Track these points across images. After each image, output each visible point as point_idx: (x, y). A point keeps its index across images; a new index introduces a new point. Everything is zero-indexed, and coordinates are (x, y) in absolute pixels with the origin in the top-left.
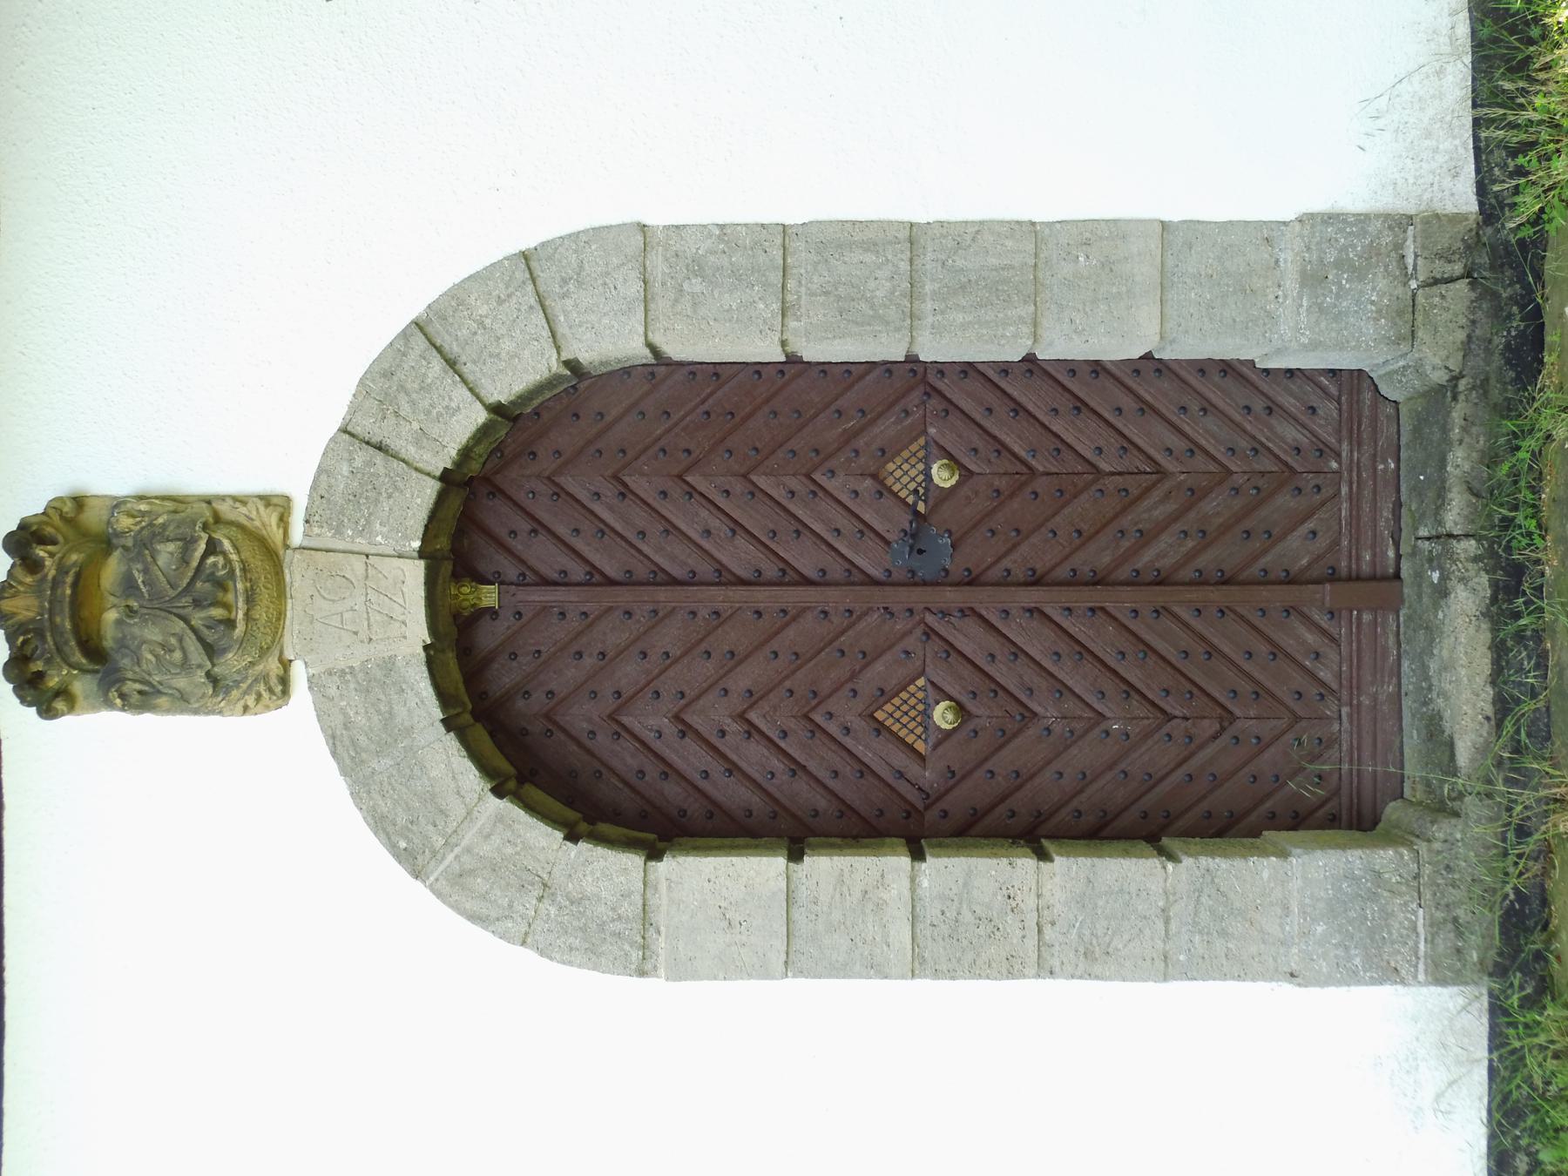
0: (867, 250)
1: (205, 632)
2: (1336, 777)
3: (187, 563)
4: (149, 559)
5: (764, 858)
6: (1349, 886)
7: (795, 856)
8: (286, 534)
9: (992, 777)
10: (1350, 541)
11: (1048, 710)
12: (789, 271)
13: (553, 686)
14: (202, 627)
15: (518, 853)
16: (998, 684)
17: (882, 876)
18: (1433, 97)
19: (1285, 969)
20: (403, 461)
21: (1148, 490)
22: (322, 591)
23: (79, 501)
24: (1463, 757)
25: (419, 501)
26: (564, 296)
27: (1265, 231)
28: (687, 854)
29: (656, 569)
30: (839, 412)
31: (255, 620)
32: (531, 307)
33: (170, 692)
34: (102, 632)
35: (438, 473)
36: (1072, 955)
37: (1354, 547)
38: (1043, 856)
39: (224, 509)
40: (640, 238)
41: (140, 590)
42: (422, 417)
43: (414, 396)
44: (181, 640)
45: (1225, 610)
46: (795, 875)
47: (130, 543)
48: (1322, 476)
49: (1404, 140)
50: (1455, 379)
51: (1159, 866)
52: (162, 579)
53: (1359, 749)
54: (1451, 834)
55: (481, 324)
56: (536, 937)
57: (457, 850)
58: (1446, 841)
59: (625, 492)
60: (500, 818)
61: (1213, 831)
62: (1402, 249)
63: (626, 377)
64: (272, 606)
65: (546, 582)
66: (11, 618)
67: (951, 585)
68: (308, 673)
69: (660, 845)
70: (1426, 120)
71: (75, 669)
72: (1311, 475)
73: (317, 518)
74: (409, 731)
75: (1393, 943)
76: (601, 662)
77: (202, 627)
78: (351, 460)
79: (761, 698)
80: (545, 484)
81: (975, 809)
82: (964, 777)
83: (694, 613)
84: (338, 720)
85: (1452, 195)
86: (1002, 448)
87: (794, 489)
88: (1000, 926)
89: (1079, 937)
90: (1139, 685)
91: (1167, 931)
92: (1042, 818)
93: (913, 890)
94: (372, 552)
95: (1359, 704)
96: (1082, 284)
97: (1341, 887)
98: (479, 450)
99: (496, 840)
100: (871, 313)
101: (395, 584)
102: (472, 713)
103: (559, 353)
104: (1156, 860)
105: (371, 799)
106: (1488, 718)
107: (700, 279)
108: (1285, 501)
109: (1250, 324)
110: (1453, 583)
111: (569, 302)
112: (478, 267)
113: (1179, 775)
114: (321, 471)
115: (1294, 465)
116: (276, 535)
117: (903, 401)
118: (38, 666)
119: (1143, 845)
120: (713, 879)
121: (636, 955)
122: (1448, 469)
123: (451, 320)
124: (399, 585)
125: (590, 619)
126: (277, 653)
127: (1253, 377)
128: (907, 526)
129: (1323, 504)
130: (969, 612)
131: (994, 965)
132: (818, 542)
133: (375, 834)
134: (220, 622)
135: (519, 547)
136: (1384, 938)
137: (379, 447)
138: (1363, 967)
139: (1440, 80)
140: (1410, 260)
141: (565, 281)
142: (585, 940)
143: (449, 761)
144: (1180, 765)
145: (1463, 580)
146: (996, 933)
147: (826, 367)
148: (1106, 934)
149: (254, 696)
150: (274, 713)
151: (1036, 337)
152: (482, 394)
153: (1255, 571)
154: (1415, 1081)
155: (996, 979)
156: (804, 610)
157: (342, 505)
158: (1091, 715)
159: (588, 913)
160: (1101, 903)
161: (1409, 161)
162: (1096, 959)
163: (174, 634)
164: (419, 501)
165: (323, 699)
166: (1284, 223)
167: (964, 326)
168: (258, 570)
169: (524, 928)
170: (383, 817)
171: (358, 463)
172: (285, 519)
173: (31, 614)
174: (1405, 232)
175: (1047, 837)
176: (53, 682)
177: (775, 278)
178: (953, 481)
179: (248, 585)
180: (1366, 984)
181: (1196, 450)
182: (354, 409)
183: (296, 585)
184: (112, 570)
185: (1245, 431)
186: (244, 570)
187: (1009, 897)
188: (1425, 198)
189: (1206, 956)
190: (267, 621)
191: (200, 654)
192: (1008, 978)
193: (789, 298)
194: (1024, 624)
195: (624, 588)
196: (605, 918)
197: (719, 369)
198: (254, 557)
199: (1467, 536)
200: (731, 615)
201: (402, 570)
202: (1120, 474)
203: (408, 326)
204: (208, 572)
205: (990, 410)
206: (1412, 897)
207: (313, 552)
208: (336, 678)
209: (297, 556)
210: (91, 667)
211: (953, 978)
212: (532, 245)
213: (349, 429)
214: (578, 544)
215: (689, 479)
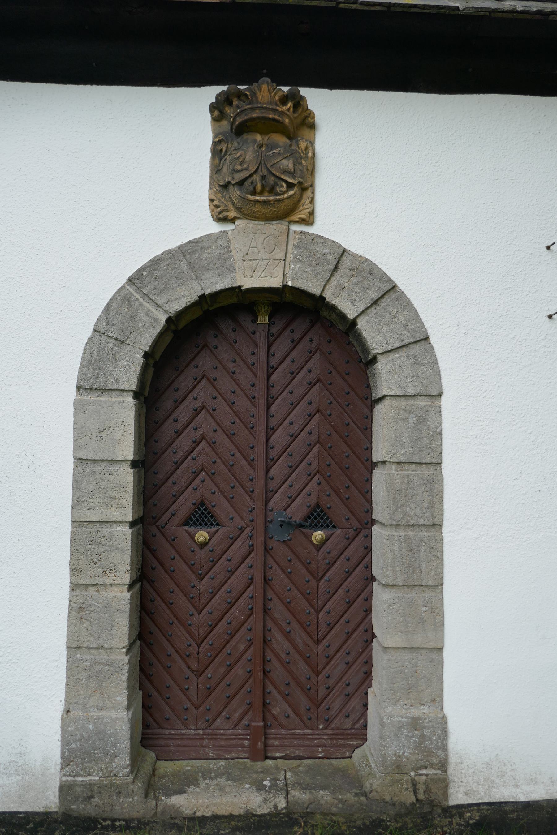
0: (429, 503)
1: (249, 181)
2: (169, 727)
3: (283, 173)
4: (285, 156)
5: (133, 449)
6: (112, 741)
7: (134, 464)
8: (296, 222)
9: (171, 559)
10: (284, 734)
11: (204, 586)
12: (419, 465)
13: (220, 348)
15: (139, 329)
16: (217, 562)
17: (123, 507)
18: (504, 782)
19: (71, 708)
20: (330, 279)
21: (309, 634)
23: (312, 127)
24: (177, 800)
25: (310, 285)
26: (408, 356)
27: (438, 699)
28: (136, 411)
29: (275, 398)
30: (348, 487)
31: (255, 205)
32: (403, 341)
33: (221, 164)
35: (324, 295)
36: (81, 601)
37: (281, 736)
38: (131, 586)
39: (309, 193)
40: (435, 393)
41: (271, 151)
42: (351, 288)
43: (361, 284)
44: (246, 169)
45: (251, 673)
46: (125, 464)
47: (293, 147)
48: (316, 721)
49: (483, 768)
50: (365, 794)
51: (125, 645)
52: (276, 161)
53: (182, 739)
54: (137, 794)
55: (395, 317)
56: (98, 337)
57: (141, 300)
58: (133, 791)
59: (311, 385)
60: (156, 320)
61: (143, 666)
62: (431, 767)
63: (366, 386)
65: (269, 346)
66: (258, 89)
67: (265, 540)
69: (142, 398)
70: (493, 778)
71: (233, 120)
72: (316, 715)
73: (303, 237)
74: (198, 278)
75: (82, 764)
76: (230, 371)
77: (252, 179)
78: (330, 254)
79: (212, 448)
80: (316, 346)
81: (156, 550)
82: (171, 545)
83: (253, 416)
84: (205, 244)
85: (457, 792)
86: (330, 565)
87: (312, 465)
88: (96, 566)
89: (90, 605)
90: (215, 631)
91: (92, 648)
92: (151, 583)
93: (115, 522)
95: (203, 739)
96: (412, 609)
97: (111, 737)
98: (334, 316)
99: (145, 318)
100: (399, 505)
102: (208, 310)
103: (380, 354)
104: (127, 643)
105: (167, 259)
106: (195, 813)
107: (415, 422)
108: (304, 702)
109: (392, 691)
110: (263, 794)
111: (405, 359)
112: (422, 316)
113: (171, 650)
114: (325, 239)
115: (321, 707)
116: (295, 217)
117: (353, 518)
118: (235, 102)
119: (136, 633)
120: (123, 423)
121: (87, 385)
122: (321, 792)
123: (397, 302)
125: (251, 367)
126: (239, 216)
127: (363, 687)
128: (294, 519)
129: (302, 721)
130: (251, 548)
131: (77, 562)
133: (150, 260)
134: (255, 188)
135: (286, 334)
136: (85, 759)
137: (336, 268)
138: (71, 748)
139: (513, 786)
140: (424, 772)
141: (415, 357)
142: (95, 361)
143: (184, 297)
144: (175, 649)
145: (265, 800)
146: (93, 563)
147: (370, 481)
148: (91, 618)
149: (218, 204)
150: (210, 215)
151: (386, 586)
152: (361, 317)
153: (270, 688)
154: (11, 774)
155: (70, 563)
156: (254, 469)
157: (309, 249)
158: (201, 608)
159: (109, 362)
160: (107, 616)
161: (473, 770)
162: (78, 613)
164: (310, 285)
165: (216, 237)
166: (442, 709)
167: (392, 551)
168: (279, 208)
169: (102, 331)
170: (158, 265)
171: (329, 257)
174: (439, 769)
175: (142, 585)
176: (228, 110)
177: (416, 459)
178: (315, 542)
179: (272, 202)
180: (62, 750)
181: (329, 659)
182: (354, 255)
183: (271, 226)
184: (281, 140)
185: (338, 683)
186: (279, 200)
187: (111, 570)
188: (455, 778)
189: (79, 668)
190: (254, 211)
191: (239, 178)
192: (70, 568)
193: (406, 465)
194: (245, 575)
195: (266, 383)
196: (106, 370)
197: (369, 430)
198: (285, 206)
199: (287, 802)
200: (252, 434)
201: (277, 277)
202: (318, 622)
203: (394, 282)
204: (279, 183)
205: (348, 560)
206: (105, 773)
207: (287, 234)
209: (285, 227)
210: (234, 127)
211: (71, 541)
212: (432, 342)
213: (345, 253)
214: (288, 361)
215: (317, 415)
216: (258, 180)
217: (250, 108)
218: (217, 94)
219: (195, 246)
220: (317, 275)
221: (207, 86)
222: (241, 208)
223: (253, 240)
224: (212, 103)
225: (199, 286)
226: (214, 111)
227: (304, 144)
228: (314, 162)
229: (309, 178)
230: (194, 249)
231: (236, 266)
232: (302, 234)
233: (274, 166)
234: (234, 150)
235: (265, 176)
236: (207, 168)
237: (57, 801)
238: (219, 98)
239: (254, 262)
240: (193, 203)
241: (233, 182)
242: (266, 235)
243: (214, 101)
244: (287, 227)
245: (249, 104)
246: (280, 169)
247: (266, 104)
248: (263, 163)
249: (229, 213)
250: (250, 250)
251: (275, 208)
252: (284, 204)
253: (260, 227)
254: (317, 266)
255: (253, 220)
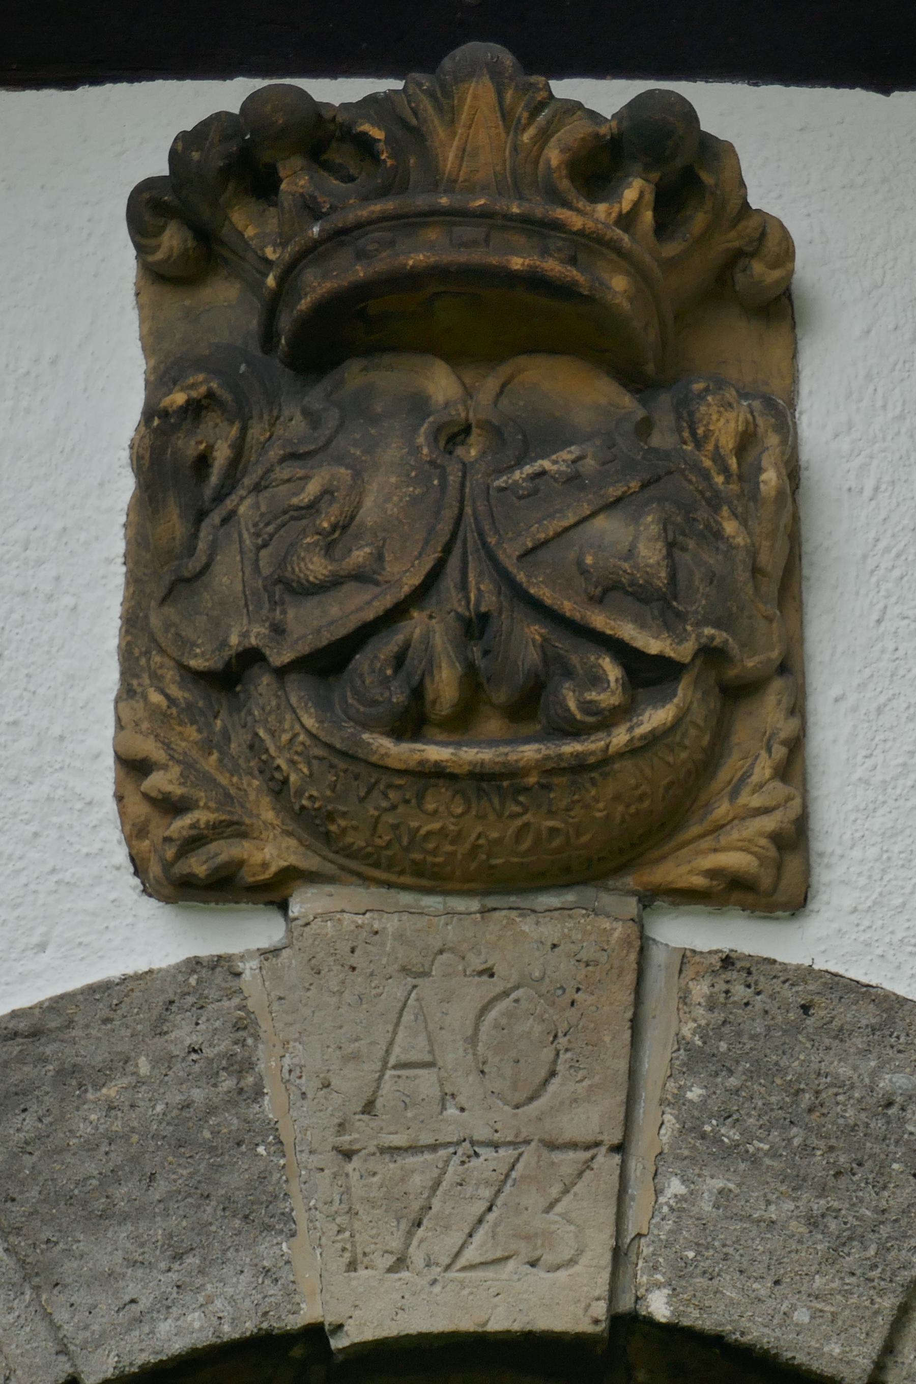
3: (598, 601)
4: (613, 492)
14: (400, 638)
22: (505, 1004)
25: (802, 1316)
31: (421, 797)
33: (202, 546)
34: (387, 359)
41: (520, 463)
44: (361, 577)
64: (462, 849)
66: (439, 108)
68: (242, 957)
71: (281, 281)
73: (740, 992)
77: (400, 638)
94: (635, 1167)
101: (528, 1238)
124: (526, 1251)
126: (311, 863)
132: (497, 108)
134: (418, 693)
149: (178, 790)
150: (121, 855)
157: (781, 1071)
163: (380, 557)
164: (802, 1316)
168: (577, 811)
172: (736, 895)
173: (450, 158)
179: (532, 780)
183: (527, 926)
198: (617, 798)
201: (572, 1262)
204: (574, 660)
207: (630, 978)
208: (224, 1045)
210: (285, 323)
216: (439, 641)
217: (385, 218)
218: (183, 137)
219: (21, 1059)
220: (841, 1244)
221: (116, 80)
222: (331, 817)
223: (407, 1017)
224: (148, 184)
225: (42, 1327)
226: (163, 229)
227: (731, 415)
228: (796, 519)
229: (769, 619)
230: (15, 1078)
231: (294, 1188)
232: (732, 975)
233: (541, 554)
234: (282, 460)
235: (484, 618)
236: (109, 561)
237: (634, 645)
238: (196, 155)
239: (411, 1160)
240: (15, 781)
241: (281, 657)
242: (497, 986)
243: (162, 168)
244: (633, 929)
245: (383, 192)
246: (584, 571)
247: (485, 189)
248: (472, 538)
249: (246, 844)
250: (387, 1087)
251: (551, 814)
252: (611, 789)
253: (451, 933)
254: (843, 1182)
255: (404, 888)
